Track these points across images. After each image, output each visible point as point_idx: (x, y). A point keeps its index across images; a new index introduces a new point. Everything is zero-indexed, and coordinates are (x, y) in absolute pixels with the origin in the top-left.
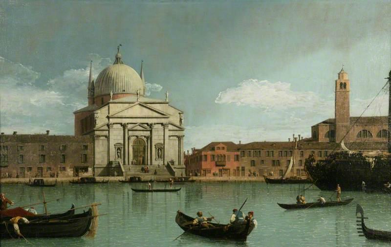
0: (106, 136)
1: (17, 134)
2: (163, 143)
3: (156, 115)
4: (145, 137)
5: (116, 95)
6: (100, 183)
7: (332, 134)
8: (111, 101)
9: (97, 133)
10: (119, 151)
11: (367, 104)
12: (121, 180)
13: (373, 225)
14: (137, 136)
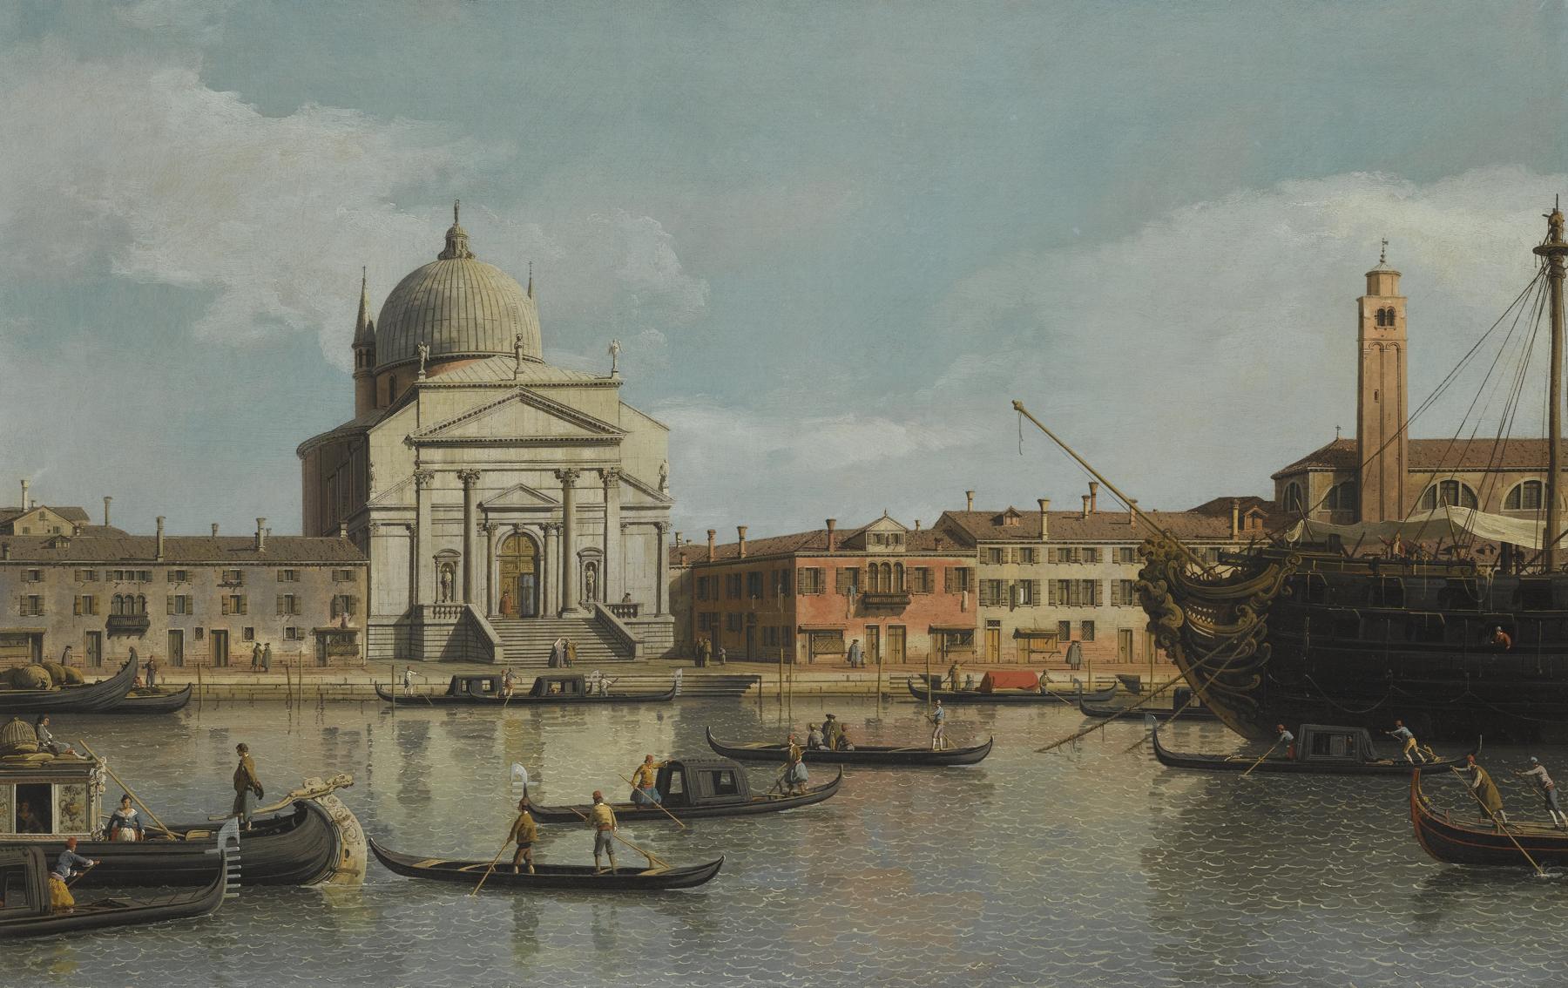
0: (408, 527)
1: (836, 527)
2: (601, 547)
3: (560, 428)
4: (540, 525)
5: (440, 360)
6: (335, 701)
7: (1347, 499)
8: (422, 379)
9: (374, 515)
10: (591, 573)
11: (1456, 401)
12: (386, 690)
13: (1168, 745)
14: (515, 526)
